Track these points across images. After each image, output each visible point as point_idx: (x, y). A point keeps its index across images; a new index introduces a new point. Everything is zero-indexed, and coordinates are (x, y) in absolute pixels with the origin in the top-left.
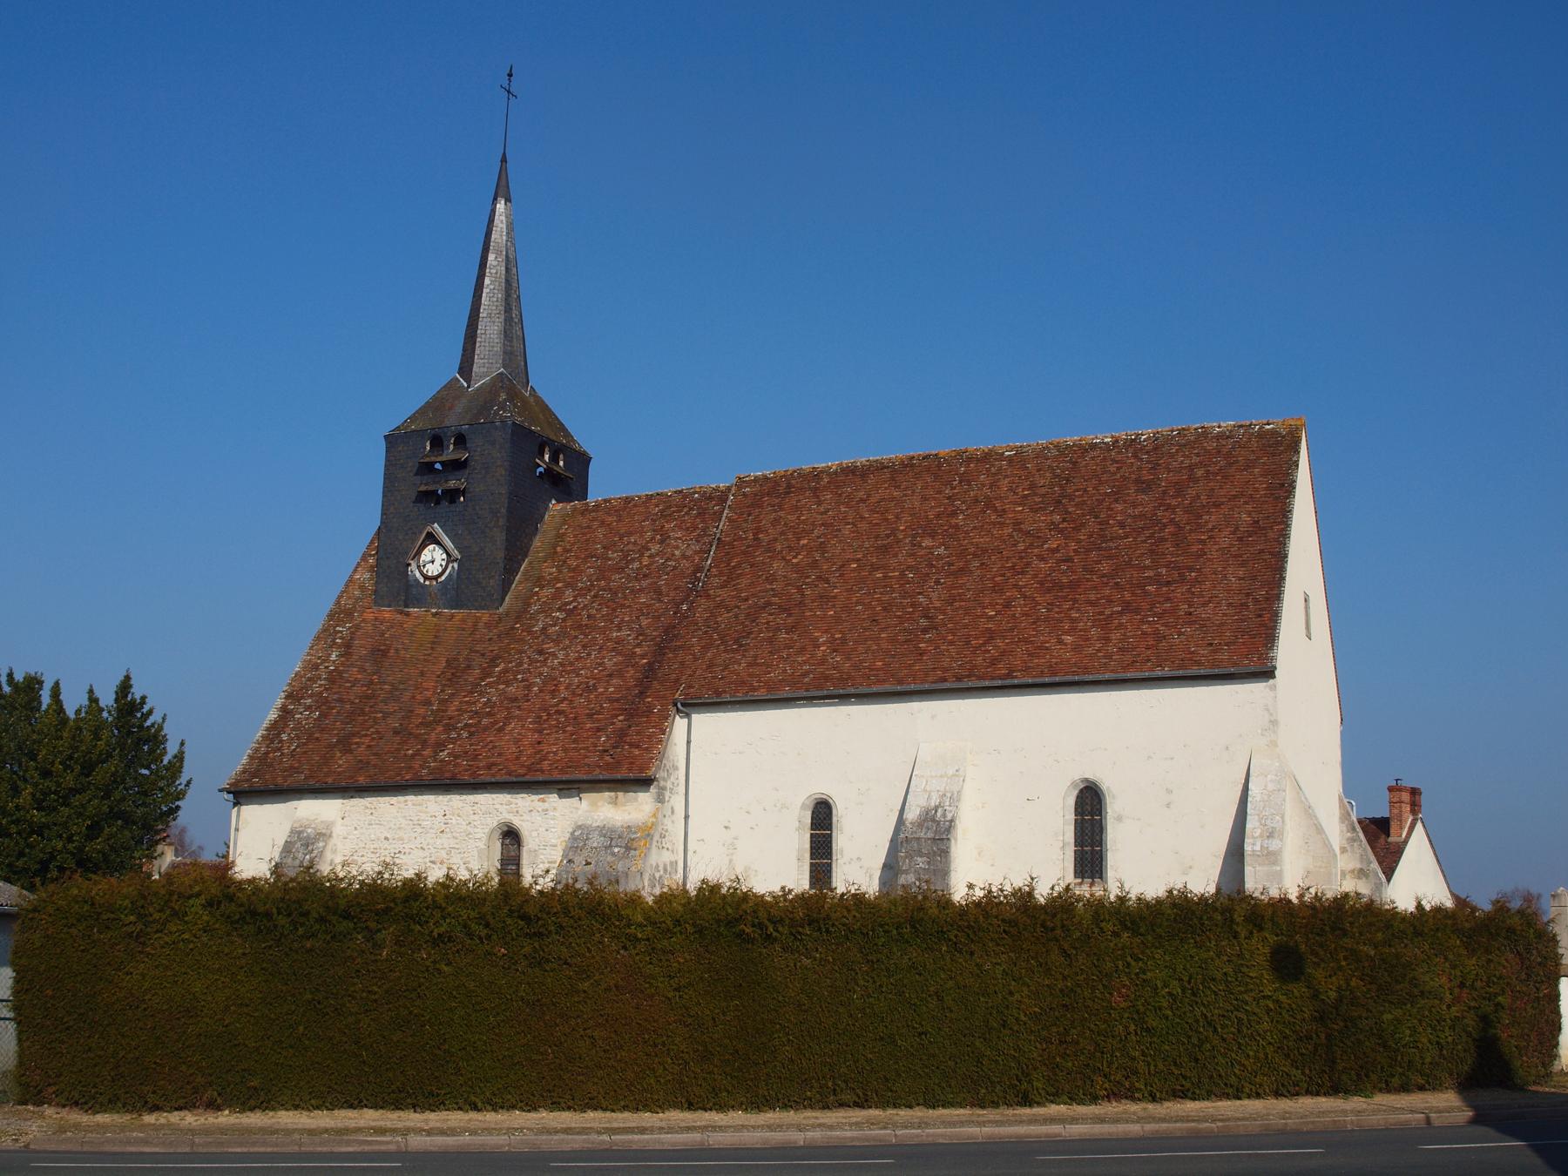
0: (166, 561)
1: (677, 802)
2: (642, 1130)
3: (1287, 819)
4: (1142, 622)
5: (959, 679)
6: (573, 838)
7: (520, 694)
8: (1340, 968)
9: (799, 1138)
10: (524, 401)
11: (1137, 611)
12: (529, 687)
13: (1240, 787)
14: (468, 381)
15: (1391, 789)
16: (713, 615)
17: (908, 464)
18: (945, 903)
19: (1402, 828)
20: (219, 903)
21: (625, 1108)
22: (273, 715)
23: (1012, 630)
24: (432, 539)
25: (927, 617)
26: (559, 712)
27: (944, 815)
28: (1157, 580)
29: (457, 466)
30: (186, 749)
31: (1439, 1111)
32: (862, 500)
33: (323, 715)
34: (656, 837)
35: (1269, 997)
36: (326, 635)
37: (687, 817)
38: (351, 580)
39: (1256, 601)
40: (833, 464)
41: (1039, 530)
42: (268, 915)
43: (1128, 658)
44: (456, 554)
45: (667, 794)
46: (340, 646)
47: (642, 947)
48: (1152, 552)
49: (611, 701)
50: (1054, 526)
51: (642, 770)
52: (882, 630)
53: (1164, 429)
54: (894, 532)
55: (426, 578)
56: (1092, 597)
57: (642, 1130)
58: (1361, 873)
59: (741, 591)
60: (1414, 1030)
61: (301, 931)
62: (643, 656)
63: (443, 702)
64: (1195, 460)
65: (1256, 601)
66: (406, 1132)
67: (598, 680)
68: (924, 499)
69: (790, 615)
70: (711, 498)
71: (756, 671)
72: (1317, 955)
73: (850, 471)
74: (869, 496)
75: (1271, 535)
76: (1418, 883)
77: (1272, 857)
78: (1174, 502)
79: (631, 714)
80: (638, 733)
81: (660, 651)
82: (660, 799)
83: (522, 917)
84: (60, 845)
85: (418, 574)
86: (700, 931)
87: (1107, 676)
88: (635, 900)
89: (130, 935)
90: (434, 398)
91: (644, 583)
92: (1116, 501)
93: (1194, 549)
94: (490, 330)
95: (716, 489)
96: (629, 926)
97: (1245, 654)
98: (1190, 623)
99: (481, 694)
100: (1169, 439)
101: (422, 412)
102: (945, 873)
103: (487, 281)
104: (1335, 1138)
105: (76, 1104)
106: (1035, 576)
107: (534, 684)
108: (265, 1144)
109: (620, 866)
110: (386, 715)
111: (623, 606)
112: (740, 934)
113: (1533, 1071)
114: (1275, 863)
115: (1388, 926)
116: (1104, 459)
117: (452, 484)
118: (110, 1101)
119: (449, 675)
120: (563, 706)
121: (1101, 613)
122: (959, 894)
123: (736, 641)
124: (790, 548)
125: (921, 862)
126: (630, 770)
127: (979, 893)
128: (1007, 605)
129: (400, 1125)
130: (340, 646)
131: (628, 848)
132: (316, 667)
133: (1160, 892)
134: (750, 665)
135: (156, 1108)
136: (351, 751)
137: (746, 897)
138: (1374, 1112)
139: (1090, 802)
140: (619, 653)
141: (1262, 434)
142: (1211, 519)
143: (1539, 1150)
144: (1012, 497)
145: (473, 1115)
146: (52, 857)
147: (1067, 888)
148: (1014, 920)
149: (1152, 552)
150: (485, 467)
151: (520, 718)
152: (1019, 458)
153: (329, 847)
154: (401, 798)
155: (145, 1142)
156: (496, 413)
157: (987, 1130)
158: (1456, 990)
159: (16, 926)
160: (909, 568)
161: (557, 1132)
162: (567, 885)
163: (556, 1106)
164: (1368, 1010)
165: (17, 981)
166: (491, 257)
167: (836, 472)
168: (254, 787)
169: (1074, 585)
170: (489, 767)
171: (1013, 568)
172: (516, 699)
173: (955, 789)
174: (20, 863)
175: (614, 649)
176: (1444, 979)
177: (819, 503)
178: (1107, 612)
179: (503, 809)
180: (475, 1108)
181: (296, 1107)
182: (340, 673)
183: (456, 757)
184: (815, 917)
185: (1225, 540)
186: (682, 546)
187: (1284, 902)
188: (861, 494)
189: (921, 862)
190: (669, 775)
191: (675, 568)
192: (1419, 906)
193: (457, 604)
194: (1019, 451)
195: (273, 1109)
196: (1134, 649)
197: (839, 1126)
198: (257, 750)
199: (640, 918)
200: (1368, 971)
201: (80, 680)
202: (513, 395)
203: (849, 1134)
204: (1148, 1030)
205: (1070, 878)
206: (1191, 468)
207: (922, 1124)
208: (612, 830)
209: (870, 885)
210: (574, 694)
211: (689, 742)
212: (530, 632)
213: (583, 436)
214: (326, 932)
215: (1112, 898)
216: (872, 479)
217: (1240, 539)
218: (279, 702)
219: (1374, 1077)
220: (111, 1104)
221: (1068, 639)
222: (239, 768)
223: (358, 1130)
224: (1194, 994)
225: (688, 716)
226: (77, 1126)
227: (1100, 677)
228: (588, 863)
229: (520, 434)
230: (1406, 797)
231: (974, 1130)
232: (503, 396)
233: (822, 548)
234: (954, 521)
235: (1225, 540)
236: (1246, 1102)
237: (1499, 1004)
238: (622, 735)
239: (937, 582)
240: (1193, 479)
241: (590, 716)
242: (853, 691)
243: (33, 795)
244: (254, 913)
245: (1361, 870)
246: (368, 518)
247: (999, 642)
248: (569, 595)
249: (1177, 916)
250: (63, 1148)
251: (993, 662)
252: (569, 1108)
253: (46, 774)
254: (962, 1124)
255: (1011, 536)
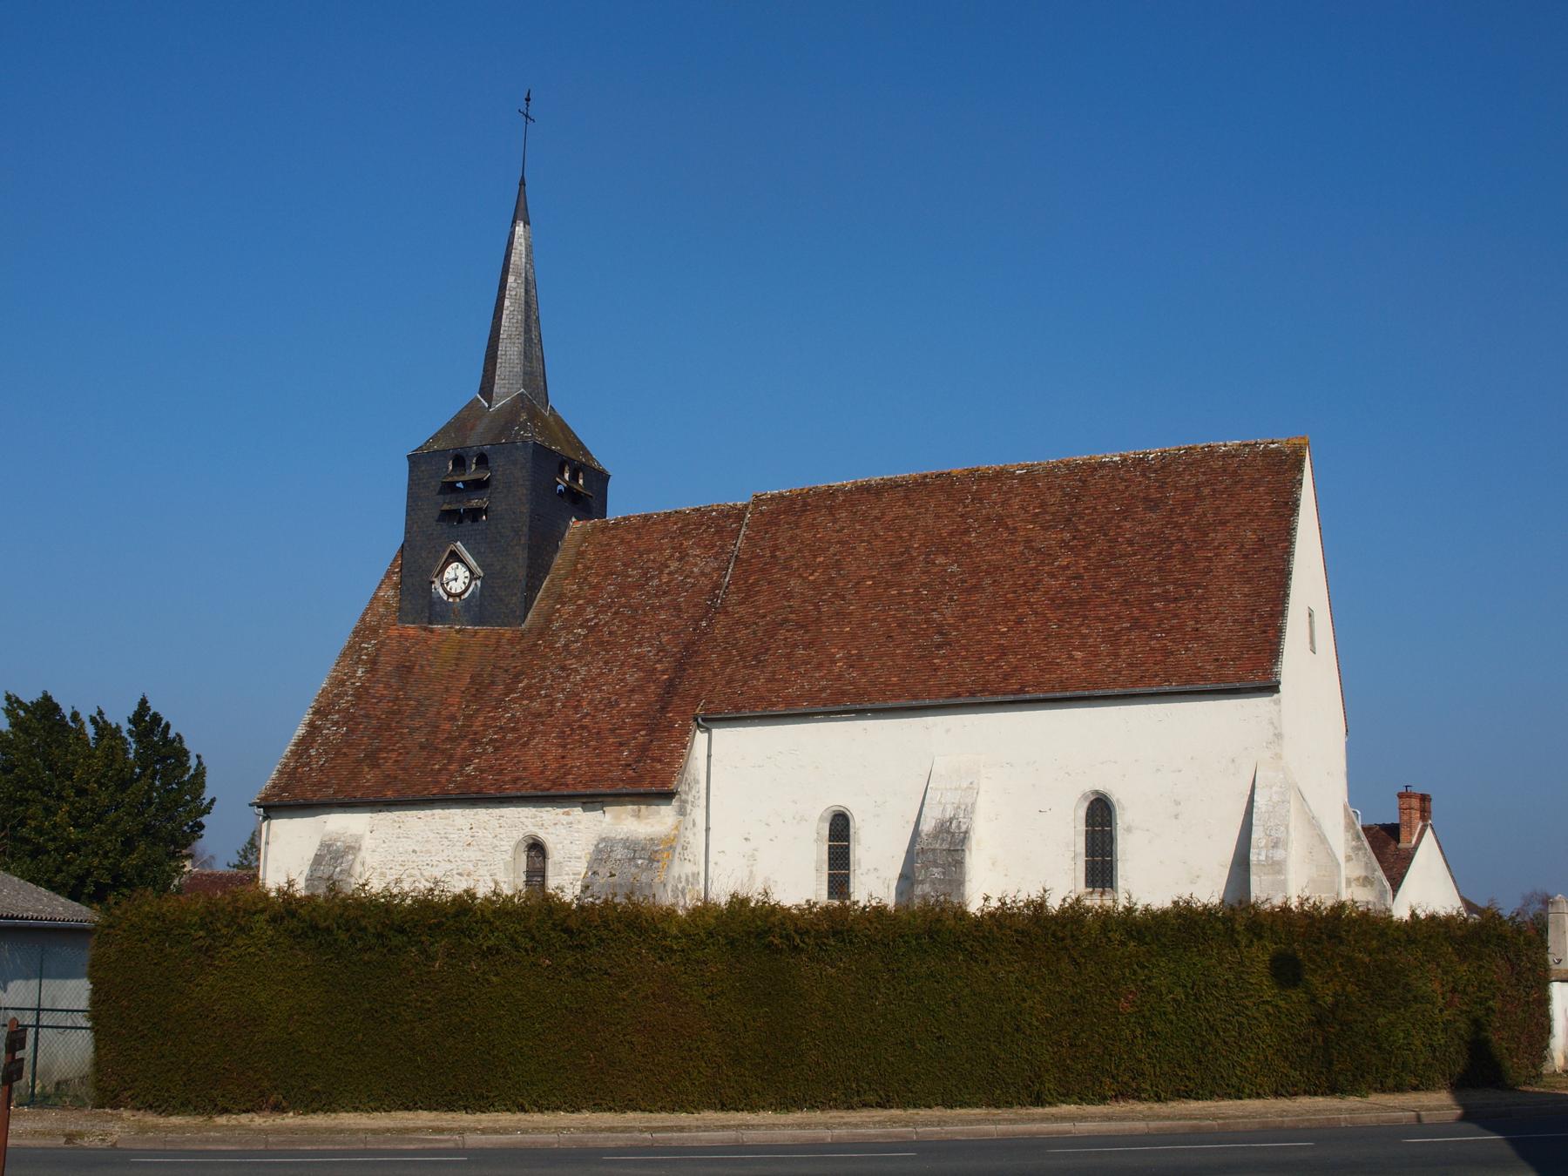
0: (200, 586)
1: (698, 814)
2: (681, 1129)
3: (1291, 830)
4: (1151, 638)
5: (973, 694)
6: (598, 850)
7: (543, 709)
8: (1336, 974)
9: (827, 1135)
10: (543, 419)
11: (1145, 627)
12: (552, 703)
13: (1246, 799)
14: (490, 403)
15: (1401, 796)
16: (732, 632)
17: (922, 483)
18: (961, 914)
19: (1411, 834)
20: (283, 918)
21: (662, 1109)
22: (301, 731)
23: (1024, 646)
24: (455, 557)
25: (941, 634)
26: (582, 727)
27: (959, 827)
28: (1164, 597)
29: (479, 485)
30: (203, 760)
31: (1430, 1109)
32: (877, 519)
33: (351, 731)
34: (679, 849)
35: (1268, 1002)
36: (352, 652)
37: (708, 829)
38: (375, 598)
39: (1261, 617)
40: (848, 482)
41: (1049, 547)
42: (328, 930)
43: (1137, 673)
44: (479, 571)
45: (689, 807)
46: (365, 663)
47: (677, 957)
48: (1160, 569)
49: (633, 716)
50: (1064, 544)
51: (664, 784)
52: (898, 646)
53: (1171, 448)
54: (907, 550)
55: (449, 595)
56: (1102, 614)
57: (681, 1129)
58: (1366, 881)
59: (758, 608)
60: (1407, 1034)
61: (359, 944)
62: (664, 672)
63: (468, 717)
64: (1202, 478)
65: (1261, 617)
66: (462, 1131)
67: (621, 695)
68: (937, 516)
69: (807, 632)
70: (728, 516)
71: (775, 686)
72: (1314, 962)
73: (865, 490)
74: (883, 514)
75: (1275, 552)
76: (1428, 890)
77: (1277, 867)
78: (1181, 520)
79: (652, 731)
80: (660, 748)
81: (680, 666)
82: (682, 812)
83: (566, 930)
84: (96, 862)
85: (441, 591)
86: (732, 943)
87: (1117, 691)
88: (670, 913)
89: (200, 949)
90: (457, 418)
91: (664, 600)
92: (1125, 519)
93: (1201, 565)
94: (510, 350)
95: (734, 507)
96: (665, 937)
97: (1249, 669)
98: (1196, 639)
99: (506, 710)
100: (1175, 458)
101: (444, 431)
102: (960, 883)
103: (507, 303)
104: (1327, 1134)
105: (151, 1107)
106: (1046, 593)
107: (557, 700)
108: (333, 1142)
109: (644, 878)
110: (412, 731)
111: (643, 622)
112: (769, 946)
113: (1524, 1072)
114: (1279, 872)
115: (1383, 934)
116: (1113, 477)
117: (475, 503)
118: (182, 1104)
119: (473, 691)
120: (586, 721)
121: (1111, 629)
122: (974, 906)
123: (755, 657)
124: (807, 566)
125: (936, 872)
126: (652, 784)
127: (994, 904)
128: (1019, 622)
129: (455, 1125)
130: (365, 663)
131: (651, 860)
132: (342, 683)
133: (1168, 904)
134: (769, 681)
135: (225, 1111)
136: (378, 766)
137: (775, 910)
138: (1367, 1110)
139: (1100, 814)
140: (640, 670)
141: (1267, 453)
142: (1219, 536)
143: (1514, 1143)
144: (1023, 515)
145: (520, 1116)
146: (89, 873)
147: (1078, 899)
148: (1029, 932)
149: (1160, 569)
150: (504, 484)
151: (544, 734)
152: (1030, 477)
153: (358, 860)
154: (428, 812)
155: (224, 1141)
156: (517, 433)
157: (1002, 1127)
158: (1448, 995)
159: (93, 941)
160: (924, 585)
161: (601, 1130)
162: (606, 901)
163: (597, 1107)
164: (1364, 1015)
165: (94, 992)
166: (511, 279)
167: (850, 491)
168: (287, 800)
169: (1083, 602)
170: (515, 781)
171: (1024, 585)
172: (540, 715)
173: (969, 801)
174: (58, 878)
175: (635, 665)
176: (1436, 986)
177: (834, 522)
178: (1117, 628)
179: (528, 822)
180: (523, 1109)
181: (356, 1109)
182: (366, 689)
183: (482, 772)
184: (836, 930)
185: (1231, 557)
186: (701, 563)
187: (1285, 909)
188: (876, 512)
189: (936, 872)
190: (690, 789)
191: (694, 585)
192: (1413, 915)
193: (480, 620)
194: (1030, 470)
195: (334, 1111)
196: (1143, 664)
197: (863, 1125)
198: (286, 765)
199: (674, 931)
200: (1362, 977)
201: (97, 694)
202: (534, 415)
203: (873, 1131)
204: (1153, 1034)
205: (1081, 888)
206: (1197, 486)
207: (941, 1122)
208: (636, 842)
209: (889, 899)
210: (596, 709)
211: (709, 756)
212: (552, 649)
213: (603, 456)
214: (383, 945)
215: (1120, 909)
216: (886, 498)
217: (1246, 557)
218: (307, 718)
219: (1369, 1078)
220: (183, 1107)
221: (1078, 654)
222: (269, 783)
223: (418, 1130)
224: (1197, 1000)
225: (708, 730)
226: (156, 1127)
227: (1109, 692)
228: (612, 875)
229: (541, 453)
230: (1415, 803)
231: (991, 1128)
232: (524, 417)
233: (838, 566)
234: (966, 539)
235: (1231, 557)
236: (1247, 1102)
237: (1489, 1008)
238: (644, 748)
239: (951, 599)
240: (1199, 497)
241: (613, 731)
242: (869, 706)
243: (69, 812)
244: (315, 928)
245: (1366, 878)
246: (393, 535)
247: (1011, 658)
248: (590, 612)
249: (1182, 927)
250: (147, 1146)
251: (1006, 677)
252: (610, 1109)
253: (81, 792)
254: (979, 1122)
255: (1022, 553)
